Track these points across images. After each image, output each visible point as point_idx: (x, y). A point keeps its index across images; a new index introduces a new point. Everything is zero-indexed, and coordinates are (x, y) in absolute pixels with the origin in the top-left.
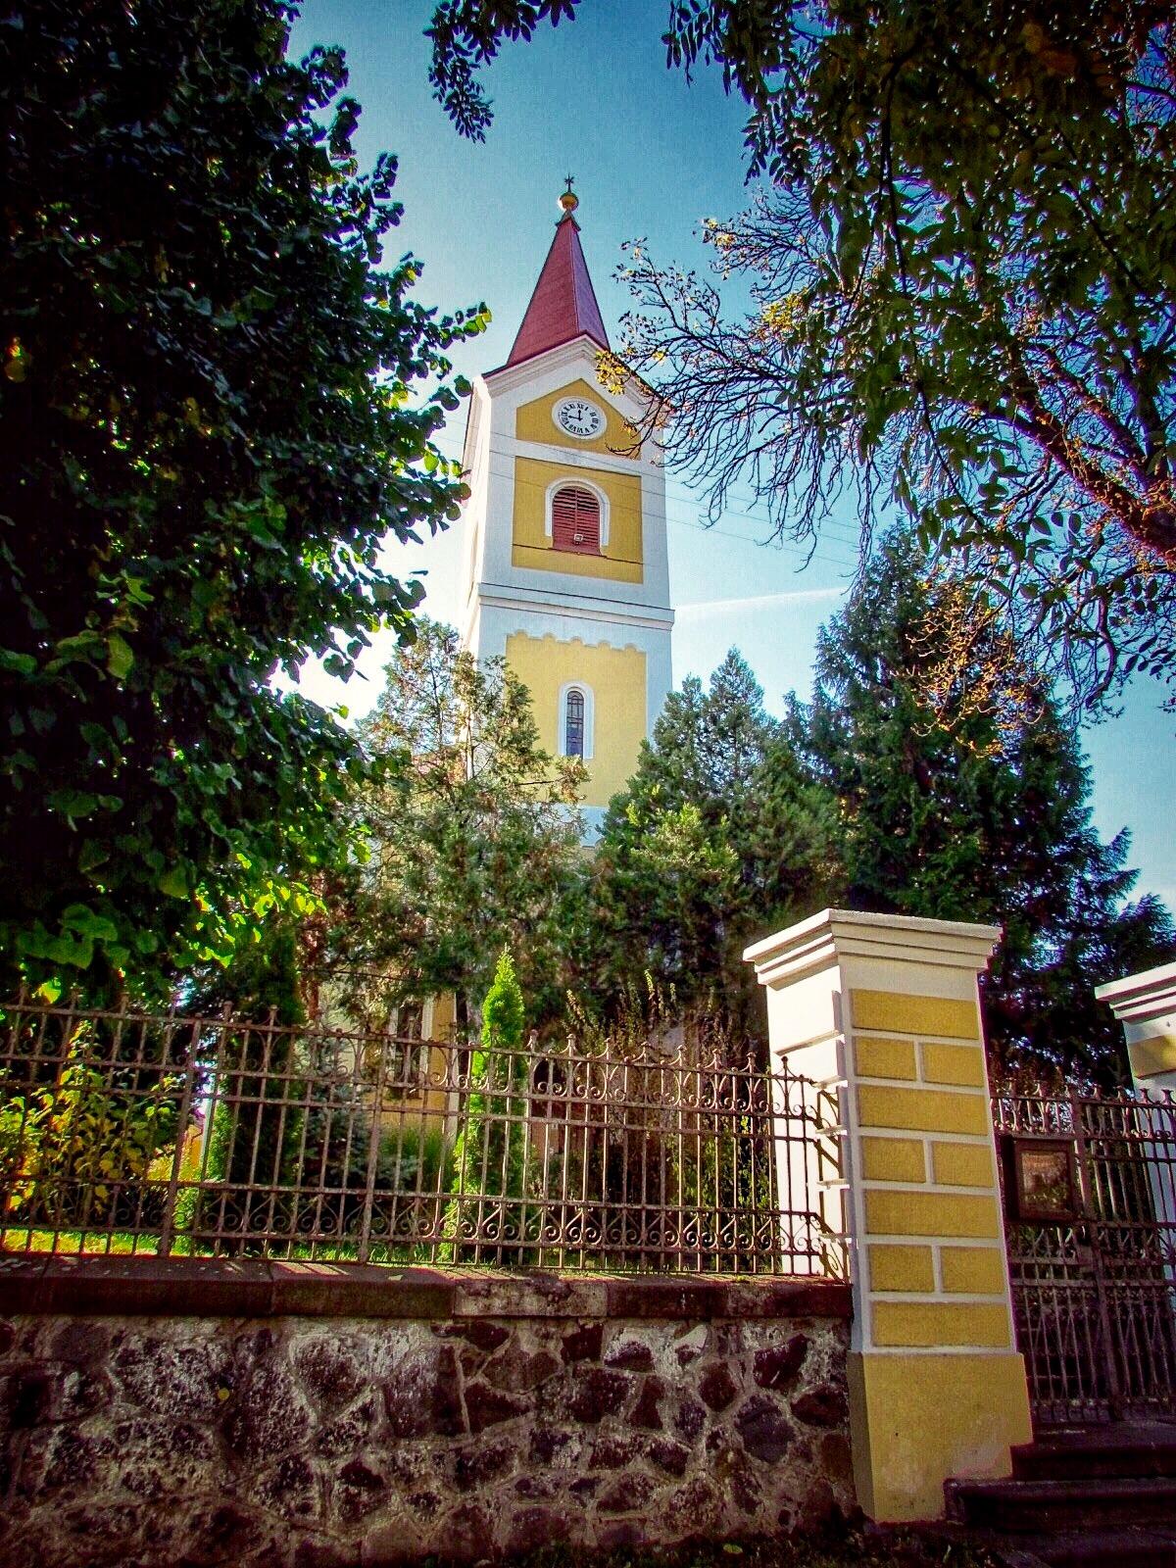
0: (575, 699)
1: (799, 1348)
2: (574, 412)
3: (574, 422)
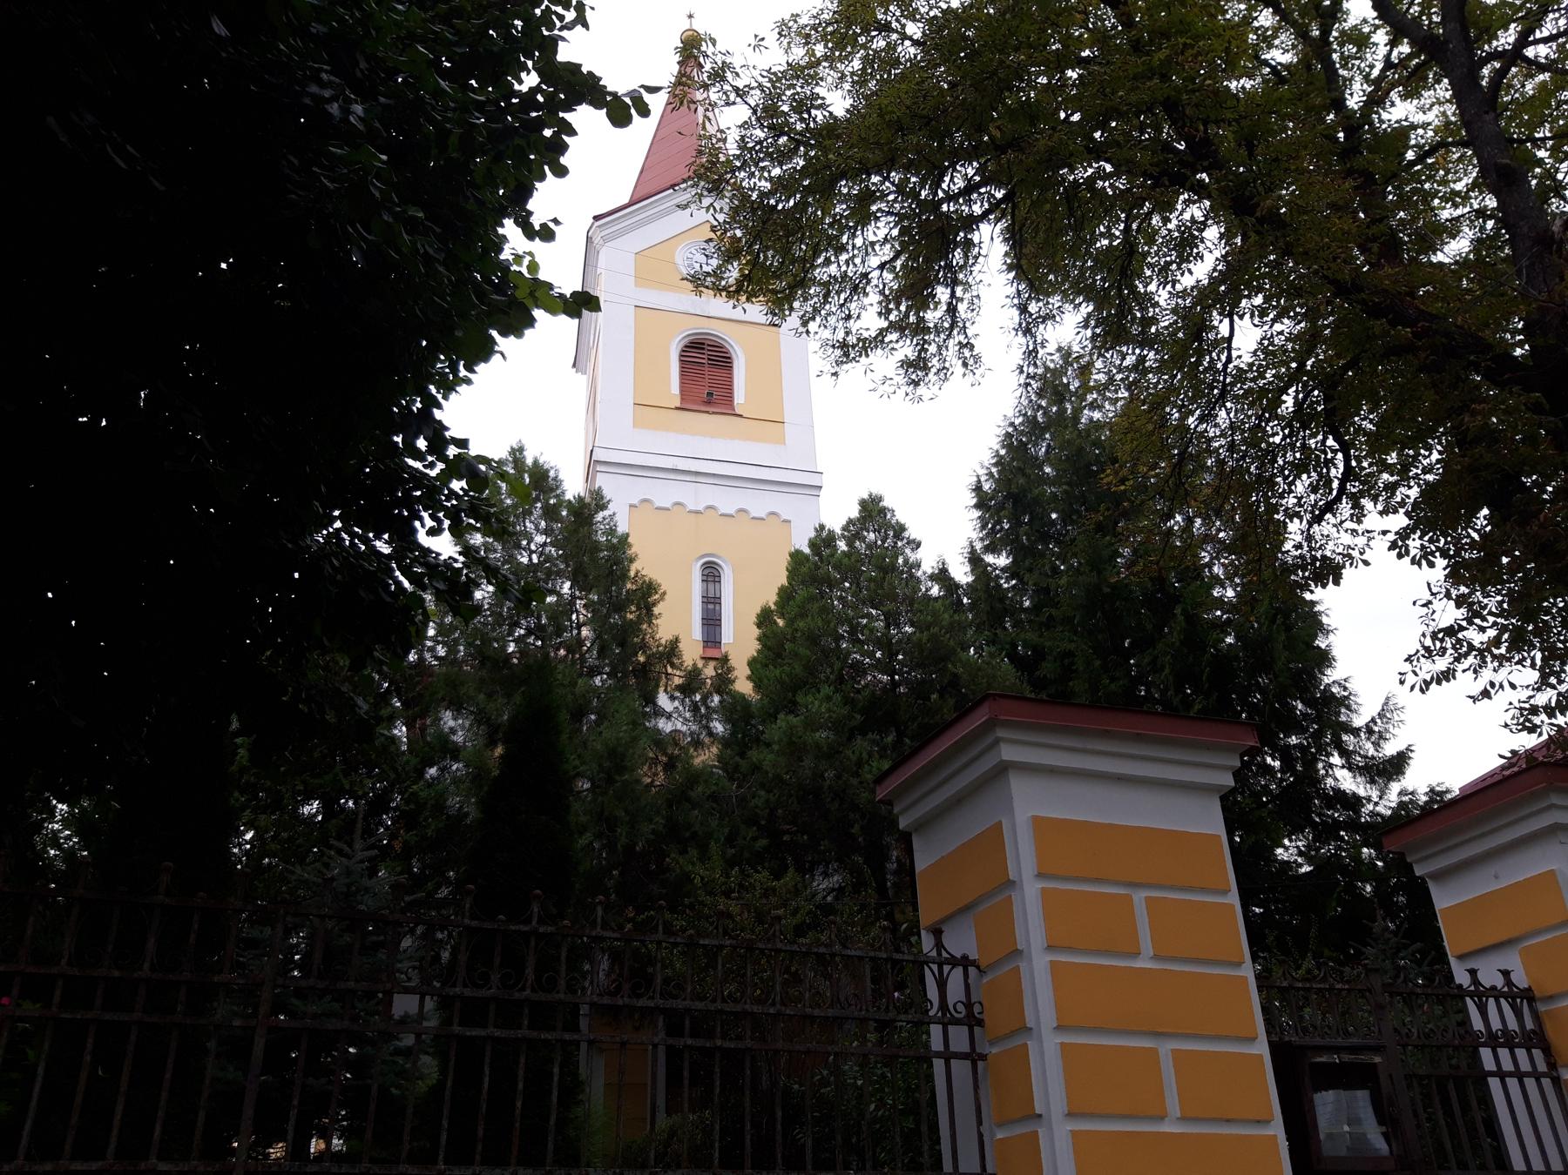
0: (711, 573)
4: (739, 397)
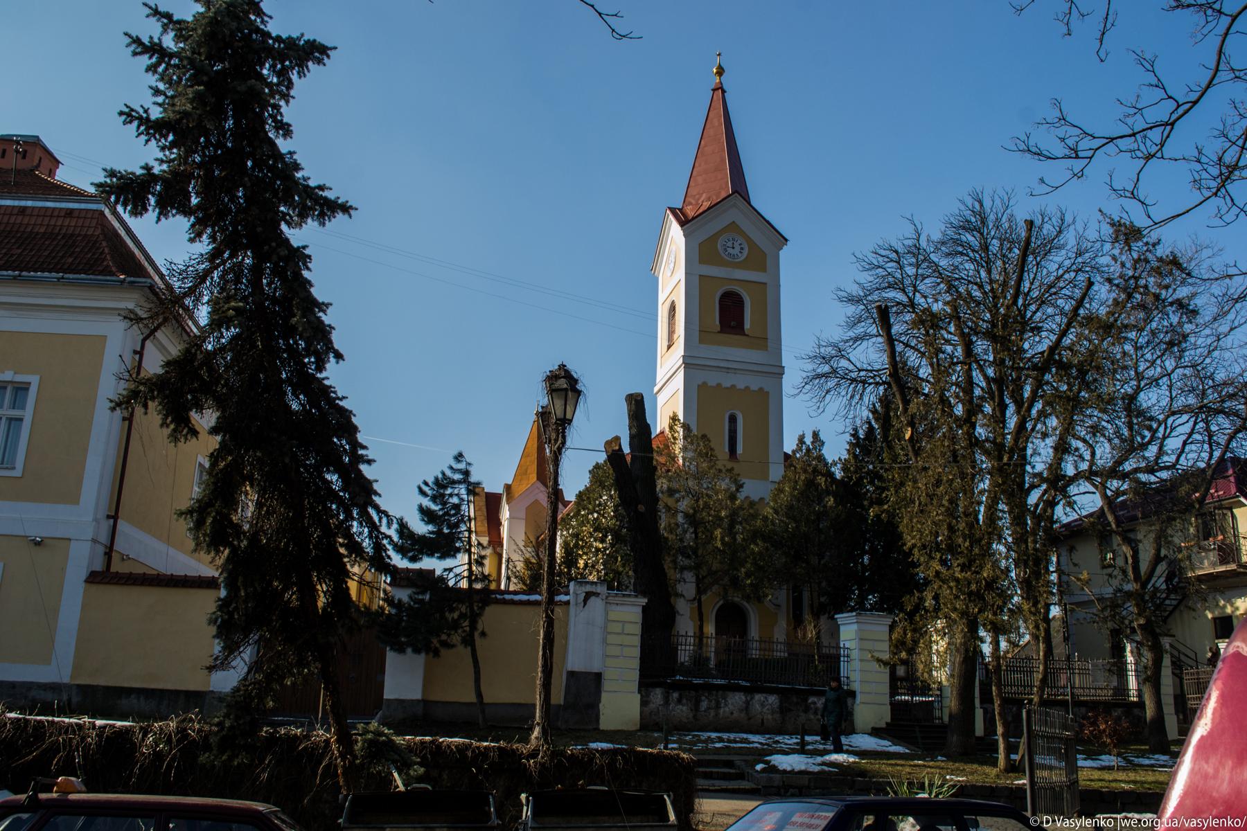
0: (733, 419)
2: (730, 244)
3: (730, 250)
4: (747, 326)
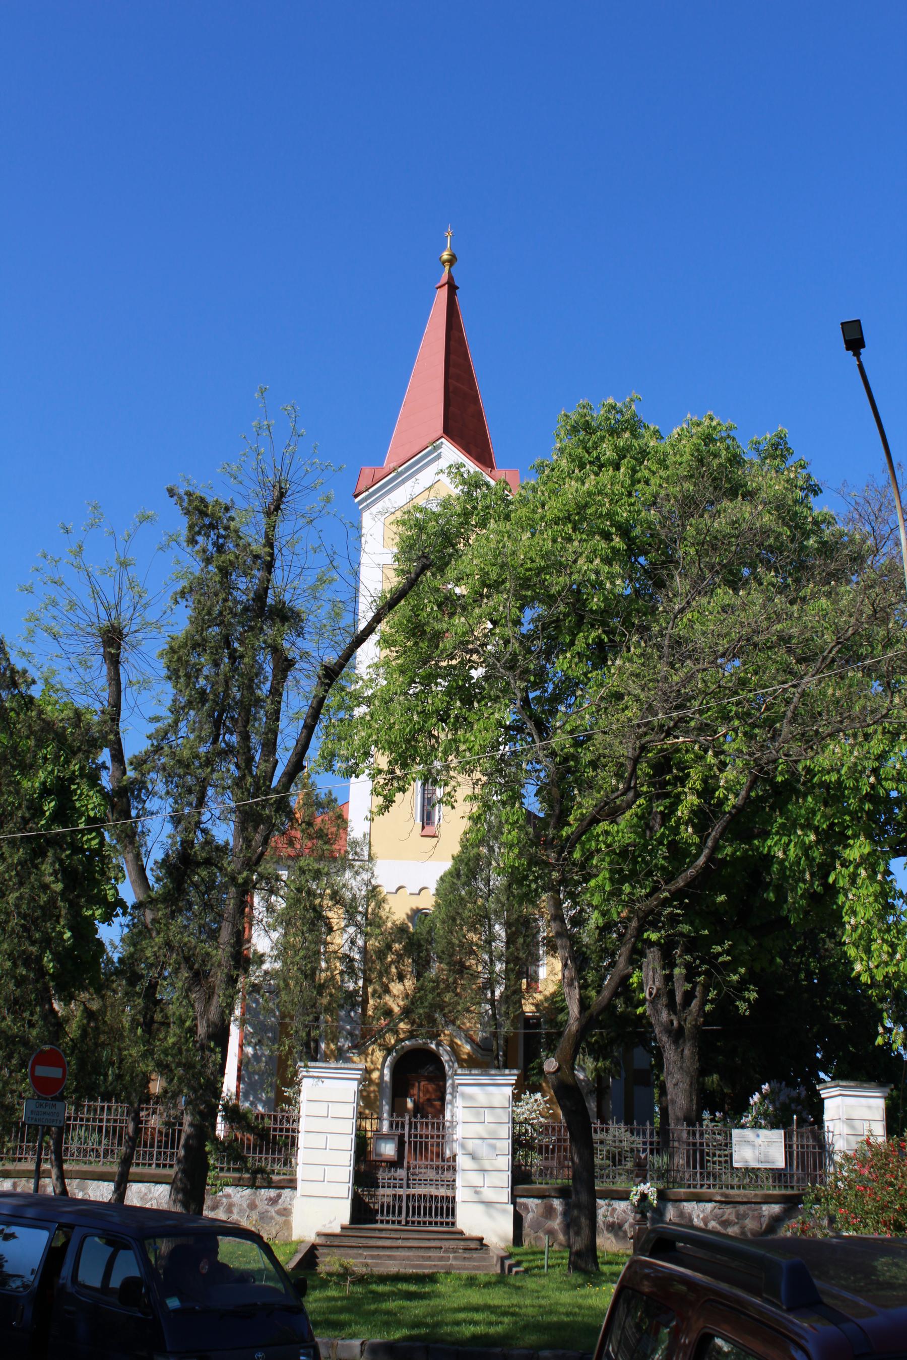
1: (279, 1196)
